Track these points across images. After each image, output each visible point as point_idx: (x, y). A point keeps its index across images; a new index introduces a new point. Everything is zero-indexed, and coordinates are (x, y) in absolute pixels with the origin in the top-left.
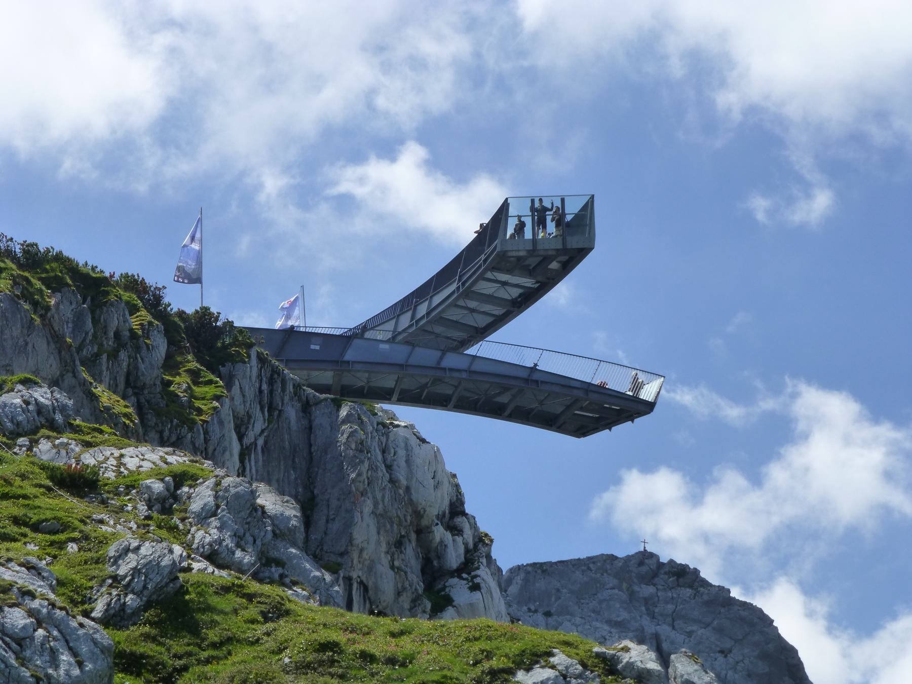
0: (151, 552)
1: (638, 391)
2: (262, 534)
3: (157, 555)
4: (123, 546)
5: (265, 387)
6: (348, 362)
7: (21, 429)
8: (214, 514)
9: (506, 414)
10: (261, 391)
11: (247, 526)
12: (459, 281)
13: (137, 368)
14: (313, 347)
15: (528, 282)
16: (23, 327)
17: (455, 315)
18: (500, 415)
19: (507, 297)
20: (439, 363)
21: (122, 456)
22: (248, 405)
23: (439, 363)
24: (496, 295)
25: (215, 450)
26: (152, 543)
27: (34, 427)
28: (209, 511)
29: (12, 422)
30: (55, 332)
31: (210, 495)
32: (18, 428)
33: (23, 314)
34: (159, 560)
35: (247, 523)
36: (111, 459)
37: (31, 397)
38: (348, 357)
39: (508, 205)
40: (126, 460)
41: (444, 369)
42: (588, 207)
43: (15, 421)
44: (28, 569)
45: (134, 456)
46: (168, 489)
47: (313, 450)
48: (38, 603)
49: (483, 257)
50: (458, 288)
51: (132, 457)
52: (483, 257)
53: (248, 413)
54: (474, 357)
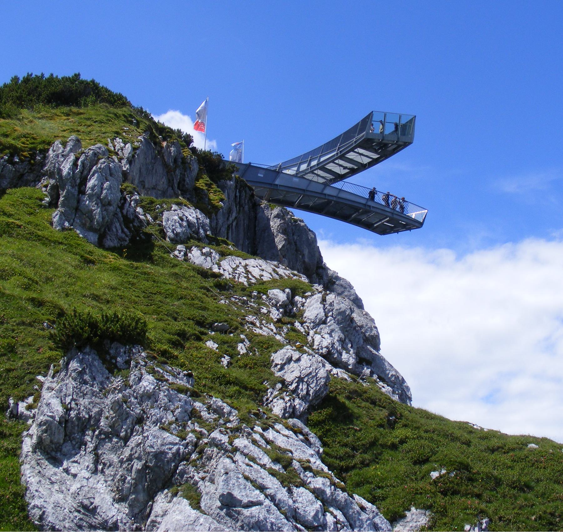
0: (310, 365)
1: (317, 193)
2: (357, 340)
3: (314, 368)
4: (287, 357)
5: (238, 194)
6: (277, 185)
7: (179, 238)
8: (324, 322)
9: (350, 220)
10: (236, 196)
11: (347, 333)
12: (338, 150)
13: (184, 180)
14: (259, 175)
15: (375, 156)
16: (152, 159)
17: (330, 166)
18: (346, 220)
19: (360, 161)
20: (323, 191)
21: (246, 265)
22: (230, 203)
23: (323, 191)
24: (354, 159)
25: (220, 229)
26: (309, 357)
27: (186, 237)
28: (320, 320)
29: (173, 232)
30: (165, 162)
31: (320, 308)
32: (177, 237)
33: (152, 150)
34: (317, 371)
35: (346, 331)
36: (240, 267)
37: (184, 215)
38: (277, 182)
39: (372, 115)
40: (250, 269)
41: (325, 195)
42: (412, 121)
43: (175, 232)
44: (295, 433)
45: (255, 266)
46: (288, 297)
47: (256, 229)
48: (321, 482)
49: (354, 140)
50: (337, 154)
51: (254, 267)
52: (354, 140)
53: (230, 207)
54: (340, 190)
